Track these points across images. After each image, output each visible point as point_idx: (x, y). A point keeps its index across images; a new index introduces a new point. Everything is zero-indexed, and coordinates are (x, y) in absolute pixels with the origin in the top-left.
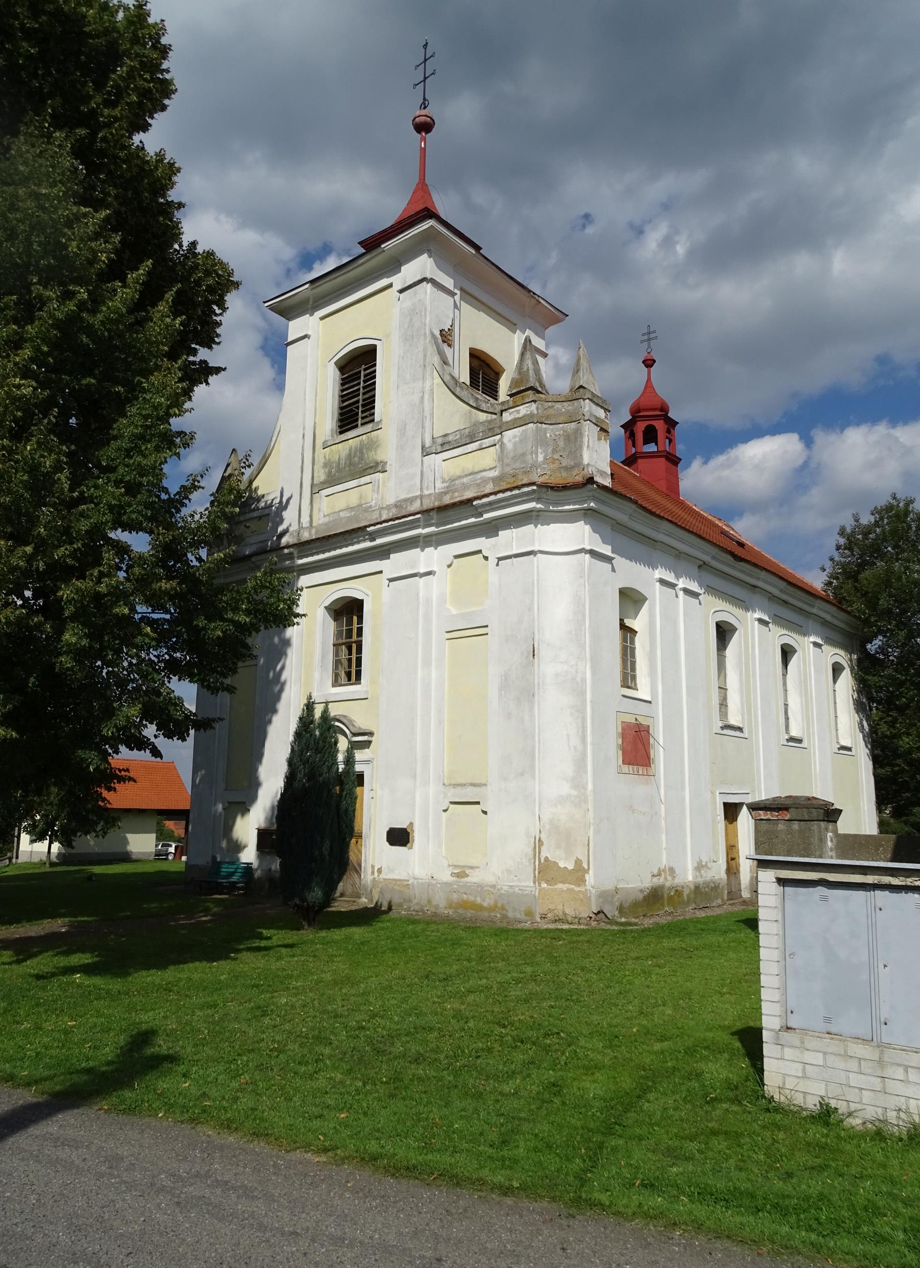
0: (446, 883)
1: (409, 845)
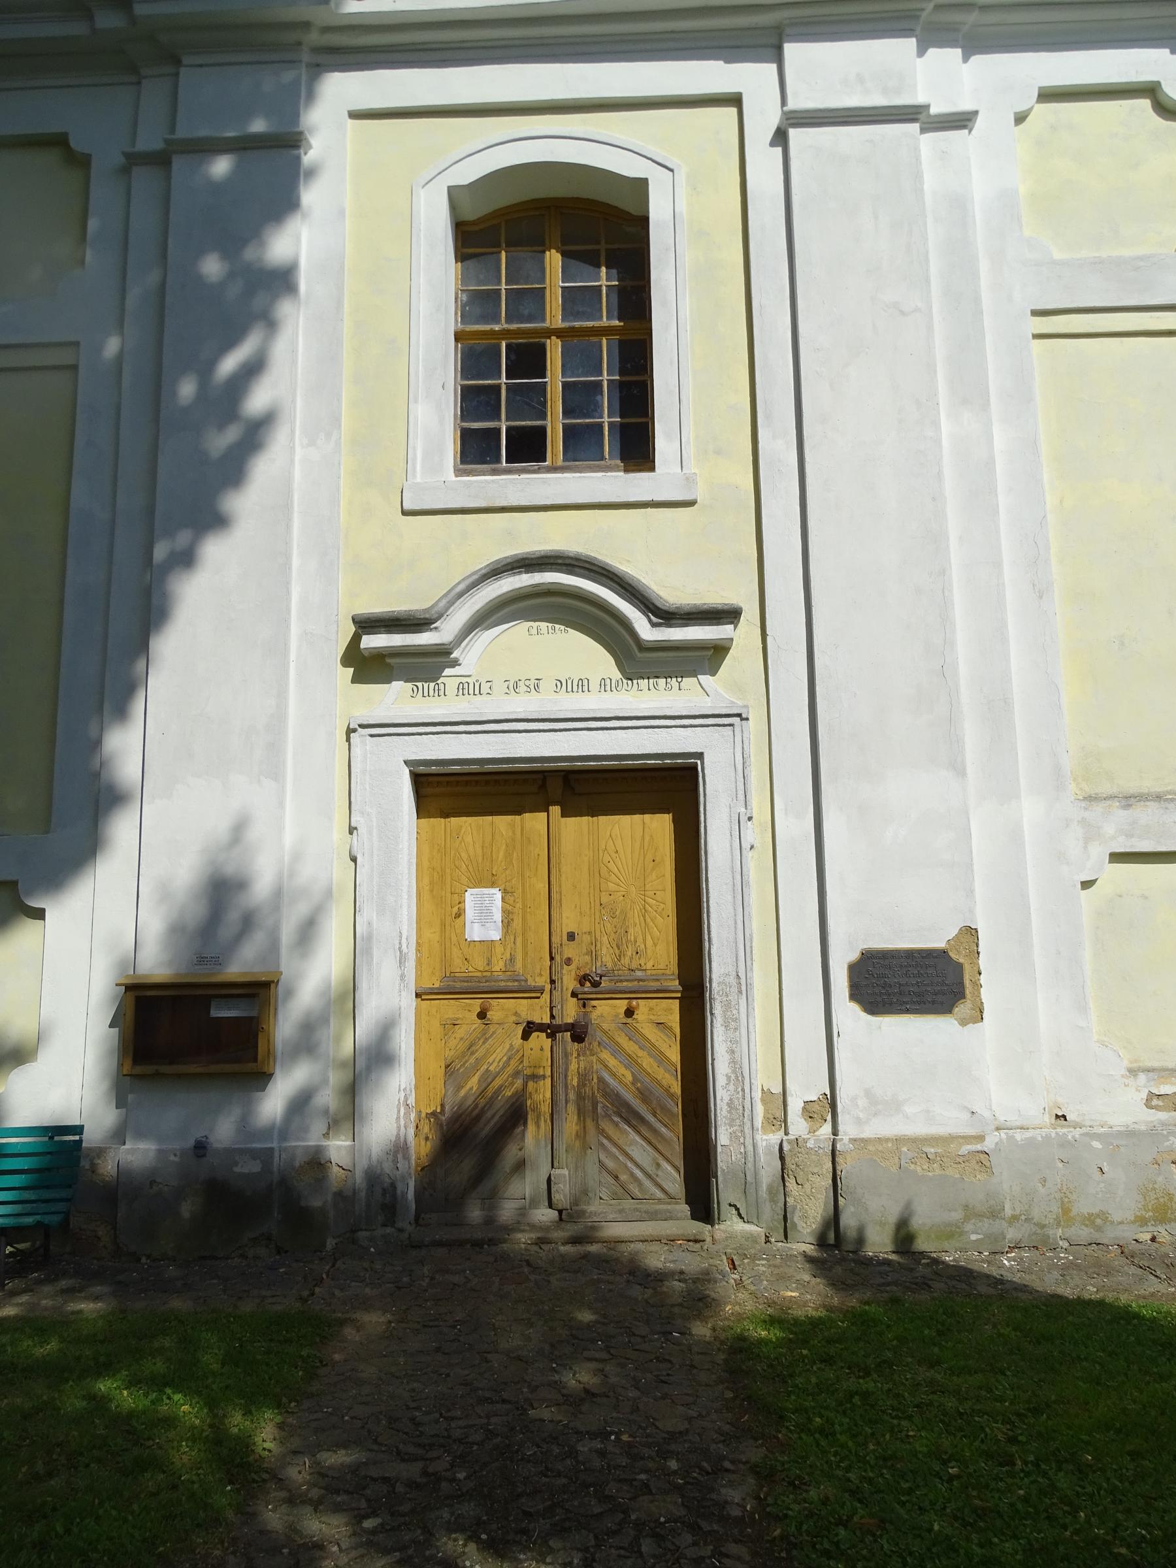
0: (1130, 1134)
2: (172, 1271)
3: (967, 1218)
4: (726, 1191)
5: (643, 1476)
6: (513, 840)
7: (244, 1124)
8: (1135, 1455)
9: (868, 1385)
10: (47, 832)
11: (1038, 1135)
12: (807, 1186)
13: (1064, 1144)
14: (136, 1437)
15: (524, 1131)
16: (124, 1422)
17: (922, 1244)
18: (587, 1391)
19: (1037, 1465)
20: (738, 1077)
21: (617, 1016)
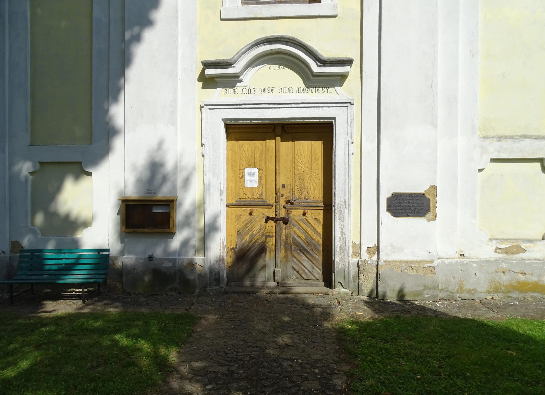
0: (488, 262)
1: (429, 215)
2: (142, 299)
3: (424, 289)
4: (337, 277)
5: (306, 375)
6: (263, 150)
7: (166, 251)
8: (486, 374)
9: (387, 346)
10: (91, 144)
11: (453, 261)
12: (367, 277)
13: (463, 264)
14: (127, 357)
15: (265, 255)
16: (124, 349)
17: (407, 298)
18: (286, 344)
19: (449, 376)
20: (344, 238)
21: (300, 215)
